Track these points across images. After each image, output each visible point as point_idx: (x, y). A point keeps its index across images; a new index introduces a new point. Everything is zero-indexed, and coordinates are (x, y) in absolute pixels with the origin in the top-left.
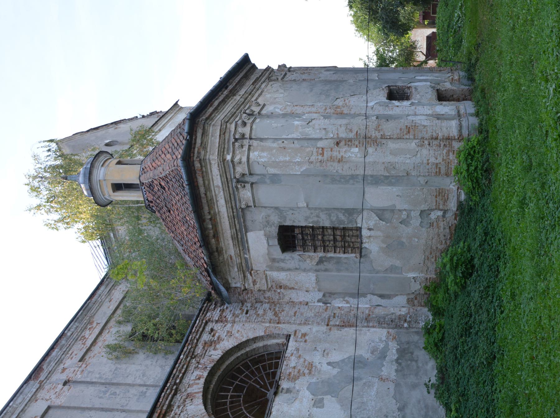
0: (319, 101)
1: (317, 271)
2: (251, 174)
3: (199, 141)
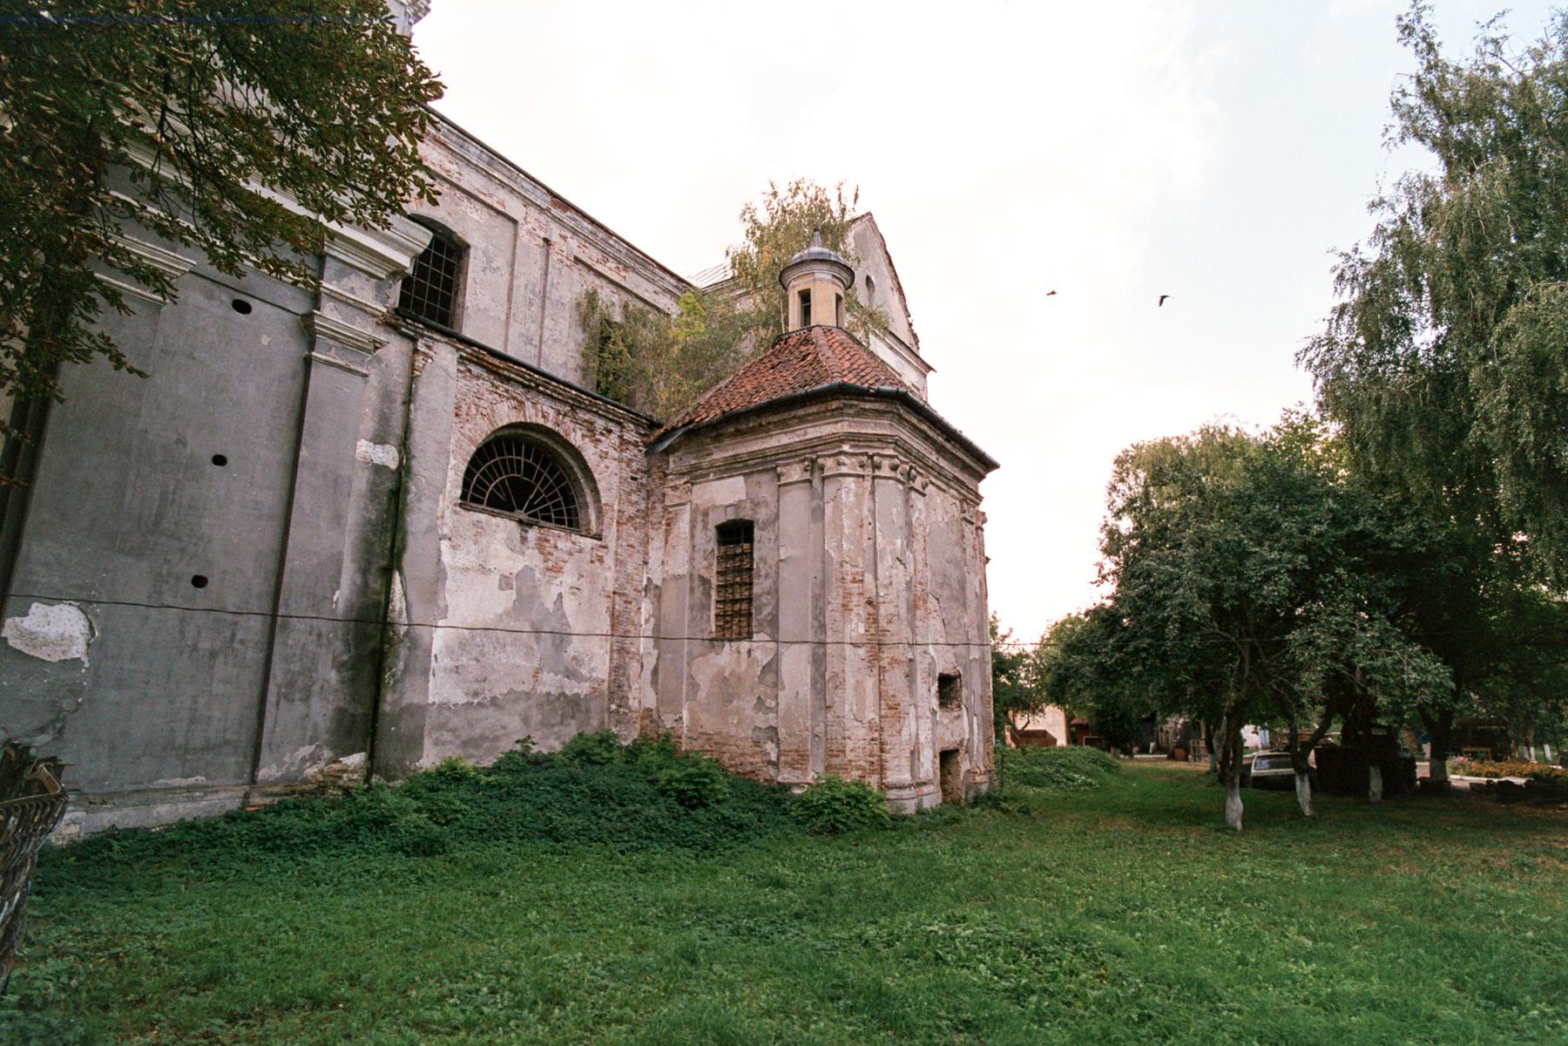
0: (934, 574)
1: (691, 575)
2: (824, 479)
3: (868, 406)
